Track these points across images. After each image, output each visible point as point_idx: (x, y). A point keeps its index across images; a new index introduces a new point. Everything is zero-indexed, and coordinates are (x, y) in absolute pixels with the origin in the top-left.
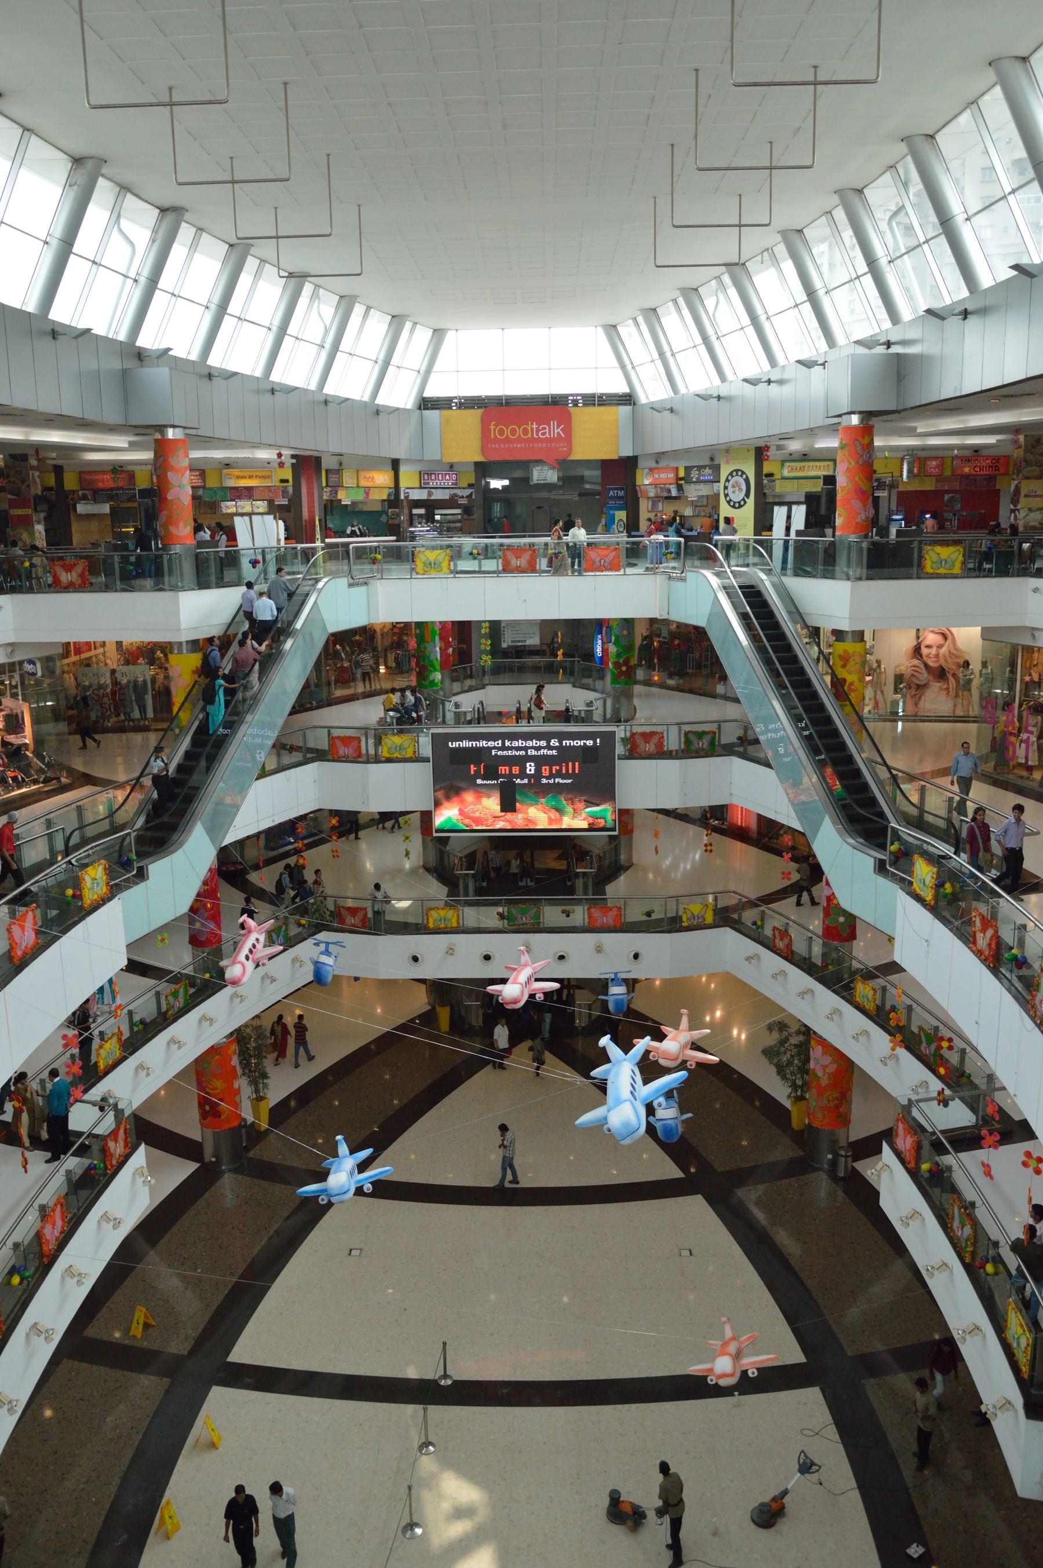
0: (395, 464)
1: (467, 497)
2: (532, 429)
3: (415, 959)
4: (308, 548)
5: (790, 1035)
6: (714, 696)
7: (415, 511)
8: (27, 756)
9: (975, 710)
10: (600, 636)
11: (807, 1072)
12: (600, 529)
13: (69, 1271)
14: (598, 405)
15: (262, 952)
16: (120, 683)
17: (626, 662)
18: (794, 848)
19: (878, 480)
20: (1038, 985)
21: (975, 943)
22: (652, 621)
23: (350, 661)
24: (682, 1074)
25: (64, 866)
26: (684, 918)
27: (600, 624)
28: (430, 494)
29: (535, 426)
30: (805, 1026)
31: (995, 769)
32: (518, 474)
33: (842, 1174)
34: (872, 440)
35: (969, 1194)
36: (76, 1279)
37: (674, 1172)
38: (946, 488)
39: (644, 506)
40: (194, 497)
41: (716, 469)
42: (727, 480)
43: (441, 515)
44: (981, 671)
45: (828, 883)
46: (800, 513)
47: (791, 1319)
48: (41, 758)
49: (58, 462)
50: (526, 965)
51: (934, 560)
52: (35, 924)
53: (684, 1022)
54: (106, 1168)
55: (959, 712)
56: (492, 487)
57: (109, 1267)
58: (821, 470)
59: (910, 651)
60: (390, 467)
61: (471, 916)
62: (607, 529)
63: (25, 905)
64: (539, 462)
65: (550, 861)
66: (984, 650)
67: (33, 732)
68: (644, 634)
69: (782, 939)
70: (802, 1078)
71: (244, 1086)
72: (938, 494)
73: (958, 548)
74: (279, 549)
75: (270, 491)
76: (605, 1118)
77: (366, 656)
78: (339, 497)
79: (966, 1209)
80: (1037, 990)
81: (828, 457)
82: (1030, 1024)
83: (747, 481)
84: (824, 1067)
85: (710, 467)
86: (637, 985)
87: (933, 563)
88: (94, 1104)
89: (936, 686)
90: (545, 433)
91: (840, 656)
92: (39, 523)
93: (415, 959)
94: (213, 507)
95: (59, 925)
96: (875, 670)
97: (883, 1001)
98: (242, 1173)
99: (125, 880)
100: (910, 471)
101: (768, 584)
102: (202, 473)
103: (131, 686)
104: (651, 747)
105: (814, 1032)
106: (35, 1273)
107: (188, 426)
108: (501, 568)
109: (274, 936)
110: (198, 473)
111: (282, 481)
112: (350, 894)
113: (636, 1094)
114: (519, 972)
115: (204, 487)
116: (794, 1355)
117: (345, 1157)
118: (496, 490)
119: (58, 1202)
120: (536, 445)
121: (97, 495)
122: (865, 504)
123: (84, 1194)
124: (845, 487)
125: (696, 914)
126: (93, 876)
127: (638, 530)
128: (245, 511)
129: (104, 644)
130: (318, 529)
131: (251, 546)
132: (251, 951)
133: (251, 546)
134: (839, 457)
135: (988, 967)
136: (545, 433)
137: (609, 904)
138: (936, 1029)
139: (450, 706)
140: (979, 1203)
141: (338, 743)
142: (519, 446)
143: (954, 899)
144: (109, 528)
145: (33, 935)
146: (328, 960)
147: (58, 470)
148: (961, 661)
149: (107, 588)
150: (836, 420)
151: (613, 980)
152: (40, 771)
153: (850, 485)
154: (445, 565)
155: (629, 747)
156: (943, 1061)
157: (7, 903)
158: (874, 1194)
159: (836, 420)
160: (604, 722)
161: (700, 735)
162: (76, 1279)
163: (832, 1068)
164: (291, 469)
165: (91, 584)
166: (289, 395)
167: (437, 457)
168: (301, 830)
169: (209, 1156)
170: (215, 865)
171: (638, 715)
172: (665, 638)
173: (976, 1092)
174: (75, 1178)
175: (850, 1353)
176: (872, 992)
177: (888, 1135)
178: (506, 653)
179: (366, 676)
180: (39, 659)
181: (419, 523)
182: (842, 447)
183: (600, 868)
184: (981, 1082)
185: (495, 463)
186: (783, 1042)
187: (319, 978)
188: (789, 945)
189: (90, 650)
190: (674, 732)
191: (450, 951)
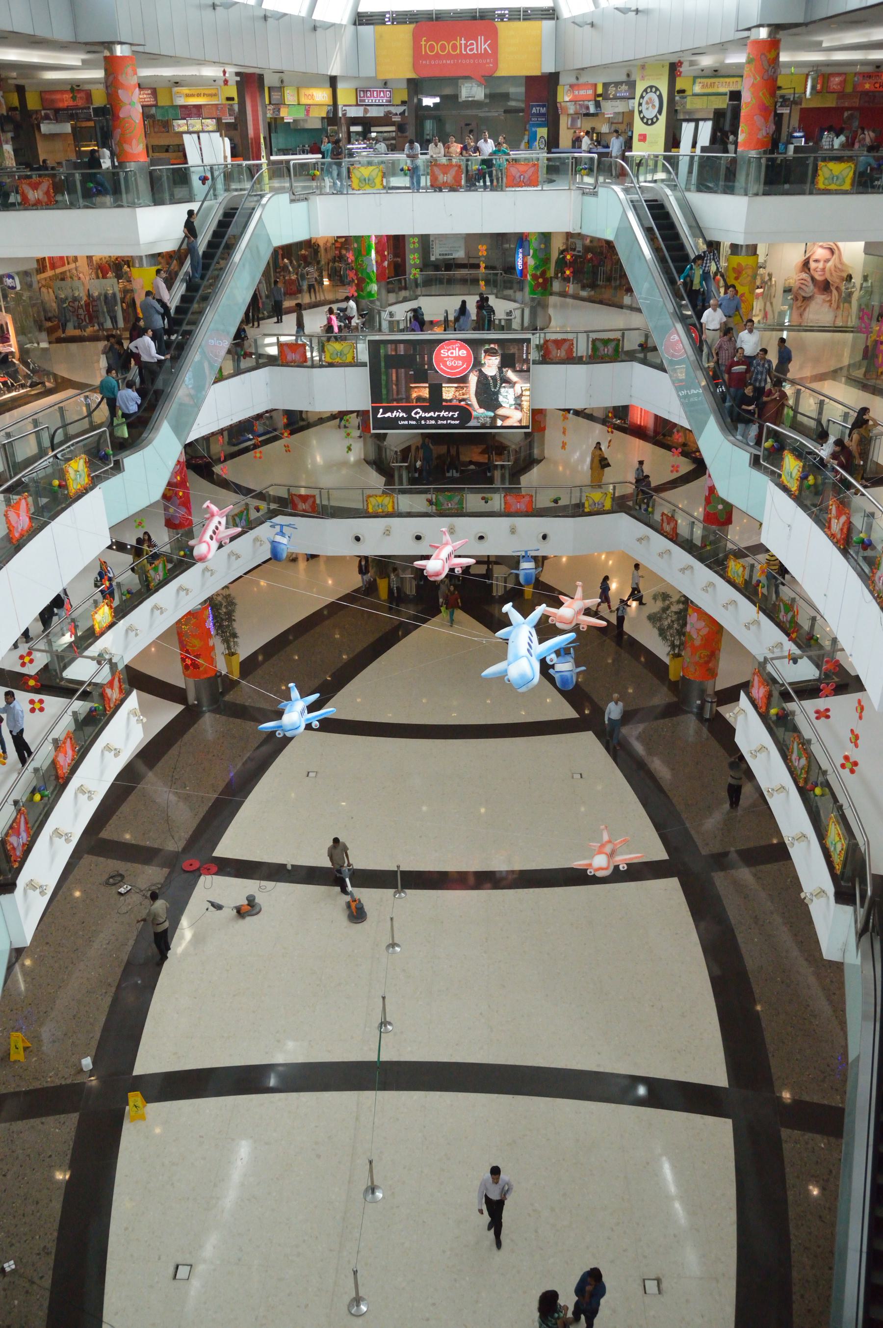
0: (333, 81)
1: (400, 114)
2: (461, 44)
3: (358, 539)
4: (254, 165)
5: (671, 603)
6: (621, 307)
7: (354, 129)
8: (14, 363)
9: (853, 321)
10: (521, 250)
11: (684, 634)
12: (523, 145)
13: (81, 790)
14: (524, 19)
15: (225, 533)
16: (93, 297)
17: (543, 273)
18: (684, 445)
19: (782, 97)
20: (879, 565)
21: (829, 528)
22: (569, 235)
23: (297, 274)
24: (572, 635)
25: (51, 460)
26: (586, 505)
27: (521, 239)
28: (366, 111)
29: (463, 42)
30: (685, 596)
31: (865, 375)
32: (448, 91)
33: (708, 716)
34: (778, 54)
35: (807, 733)
36: (87, 795)
37: (569, 712)
38: (846, 105)
39: (564, 122)
40: (146, 116)
41: (632, 85)
42: (642, 97)
43: (377, 132)
44: (862, 284)
45: (710, 476)
46: (706, 129)
47: (658, 827)
48: (26, 365)
49: (20, 82)
50: (447, 544)
51: (827, 176)
52: (28, 510)
53: (579, 593)
54: (105, 710)
55: (839, 323)
56: (424, 104)
57: (113, 787)
58: (725, 86)
59: (800, 265)
60: (328, 85)
61: (405, 502)
62: (529, 146)
63: (18, 494)
64: (467, 78)
65: (474, 455)
66: (865, 264)
67: (18, 342)
68: (561, 248)
69: (668, 524)
70: (680, 639)
71: (217, 642)
72: (839, 110)
73: (850, 164)
74: (226, 166)
75: (217, 109)
76: (506, 671)
77: (310, 269)
78: (282, 115)
79: (803, 744)
80: (878, 569)
81: (735, 73)
82: (869, 597)
83: (660, 97)
84: (698, 630)
85: (627, 83)
86: (546, 562)
87: (826, 179)
88: (92, 658)
89: (820, 298)
90: (471, 50)
91: (734, 269)
92: (7, 143)
93: (358, 539)
94: (166, 125)
95: (49, 512)
96: (766, 283)
97: (751, 577)
98: (220, 713)
99: (104, 472)
100: (813, 87)
101: (672, 199)
102: (154, 92)
103: (102, 298)
104: (561, 353)
105: (692, 602)
106: (53, 791)
107: (135, 42)
108: (429, 184)
109: (237, 520)
110: (149, 92)
111: (229, 99)
112: (303, 484)
113: (532, 651)
114: (441, 550)
115: (156, 106)
116: (659, 853)
117: (297, 700)
118: (428, 107)
119: (68, 736)
120: (464, 61)
121: (59, 115)
122: (766, 119)
123: (88, 730)
124: (749, 103)
125: (596, 501)
126: (76, 468)
127: (557, 146)
128: (195, 129)
129: (76, 259)
130: (263, 146)
131: (200, 163)
132: (214, 533)
133: (200, 163)
134: (746, 72)
135: (839, 548)
136: (471, 50)
137: (523, 493)
138: (793, 600)
139: (385, 315)
140: (814, 740)
141: (286, 349)
142: (448, 62)
143: (817, 491)
144: (73, 147)
145: (27, 519)
146: (284, 540)
147: (21, 90)
148: (845, 275)
149: (72, 206)
150: (746, 34)
151: (523, 557)
152: (27, 376)
153: (754, 101)
154: (378, 181)
155: (542, 353)
156: (797, 627)
157: (4, 492)
158: (732, 731)
159: (746, 34)
160: (522, 330)
161: (605, 342)
162: (87, 795)
163: (704, 632)
164: (235, 87)
165: (57, 201)
166: (230, 10)
167: (372, 74)
168: (259, 427)
169: (192, 699)
170: (183, 459)
171: (553, 323)
172: (579, 252)
173: (822, 652)
174: (81, 717)
175: (704, 852)
176: (741, 569)
177: (746, 686)
178: (436, 266)
179: (311, 287)
180: (18, 273)
181: (357, 140)
182: (749, 62)
183: (516, 461)
184: (827, 644)
185: (431, 79)
186: (665, 610)
187: (275, 556)
188: (675, 529)
189: (63, 265)
190: (582, 338)
191: (387, 532)
